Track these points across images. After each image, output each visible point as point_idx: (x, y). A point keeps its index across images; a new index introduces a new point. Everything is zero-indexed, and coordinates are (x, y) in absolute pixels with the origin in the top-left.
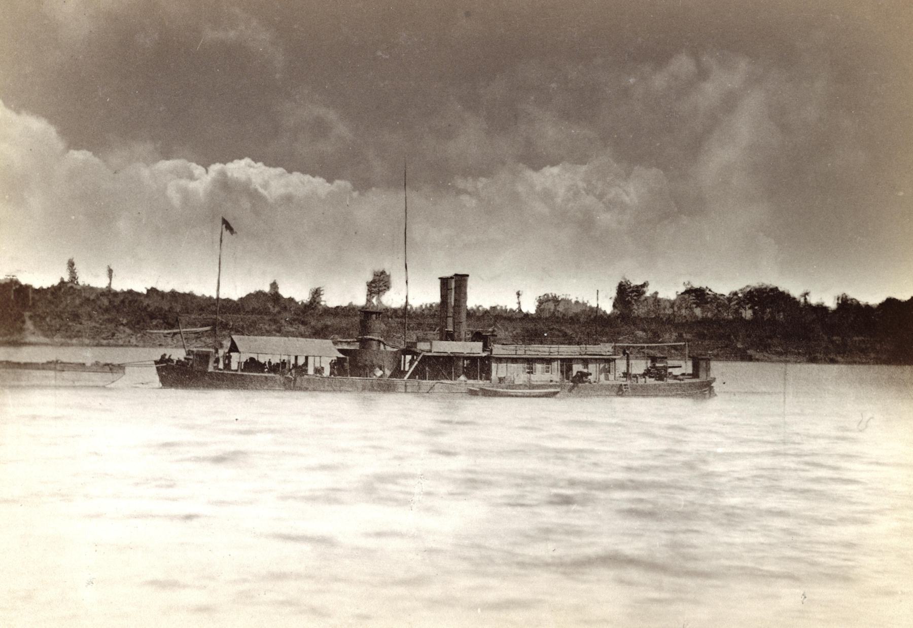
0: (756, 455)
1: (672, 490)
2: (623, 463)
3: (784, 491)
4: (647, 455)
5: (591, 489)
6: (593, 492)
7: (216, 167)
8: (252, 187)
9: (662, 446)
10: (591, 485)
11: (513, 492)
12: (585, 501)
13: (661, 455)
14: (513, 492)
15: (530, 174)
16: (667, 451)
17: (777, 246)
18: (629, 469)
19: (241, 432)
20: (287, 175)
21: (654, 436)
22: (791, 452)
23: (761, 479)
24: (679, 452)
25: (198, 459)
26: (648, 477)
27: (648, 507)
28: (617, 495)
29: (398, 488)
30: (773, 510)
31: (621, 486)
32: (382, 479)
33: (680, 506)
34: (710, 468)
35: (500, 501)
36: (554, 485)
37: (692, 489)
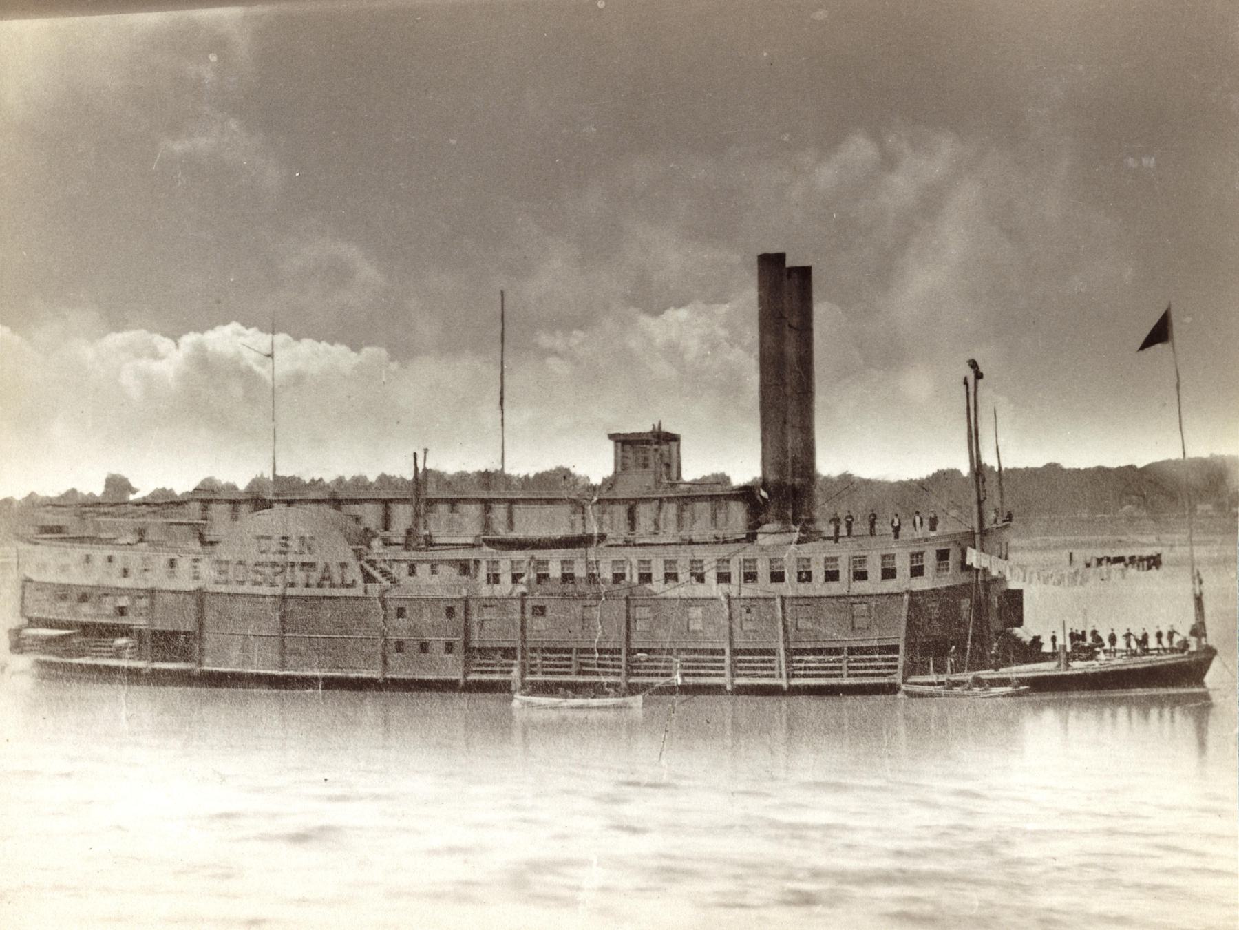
0: (1085, 834)
1: (960, 885)
2: (891, 845)
3: (1125, 886)
4: (924, 832)
5: (841, 882)
6: (847, 887)
7: (190, 339)
8: (243, 364)
9: (945, 819)
10: (842, 876)
11: (729, 886)
12: (834, 900)
13: (944, 834)
14: (729, 886)
15: (645, 321)
16: (954, 827)
17: (1012, 406)
18: (899, 853)
19: (331, 799)
20: (294, 343)
21: (935, 806)
22: (1135, 830)
23: (1091, 870)
24: (970, 829)
25: (264, 837)
26: (925, 866)
27: (928, 909)
28: (882, 891)
29: (561, 880)
30: (1109, 914)
31: (887, 878)
32: (537, 867)
33: (972, 908)
34: (1015, 853)
35: (710, 900)
36: (789, 877)
37: (988, 883)
